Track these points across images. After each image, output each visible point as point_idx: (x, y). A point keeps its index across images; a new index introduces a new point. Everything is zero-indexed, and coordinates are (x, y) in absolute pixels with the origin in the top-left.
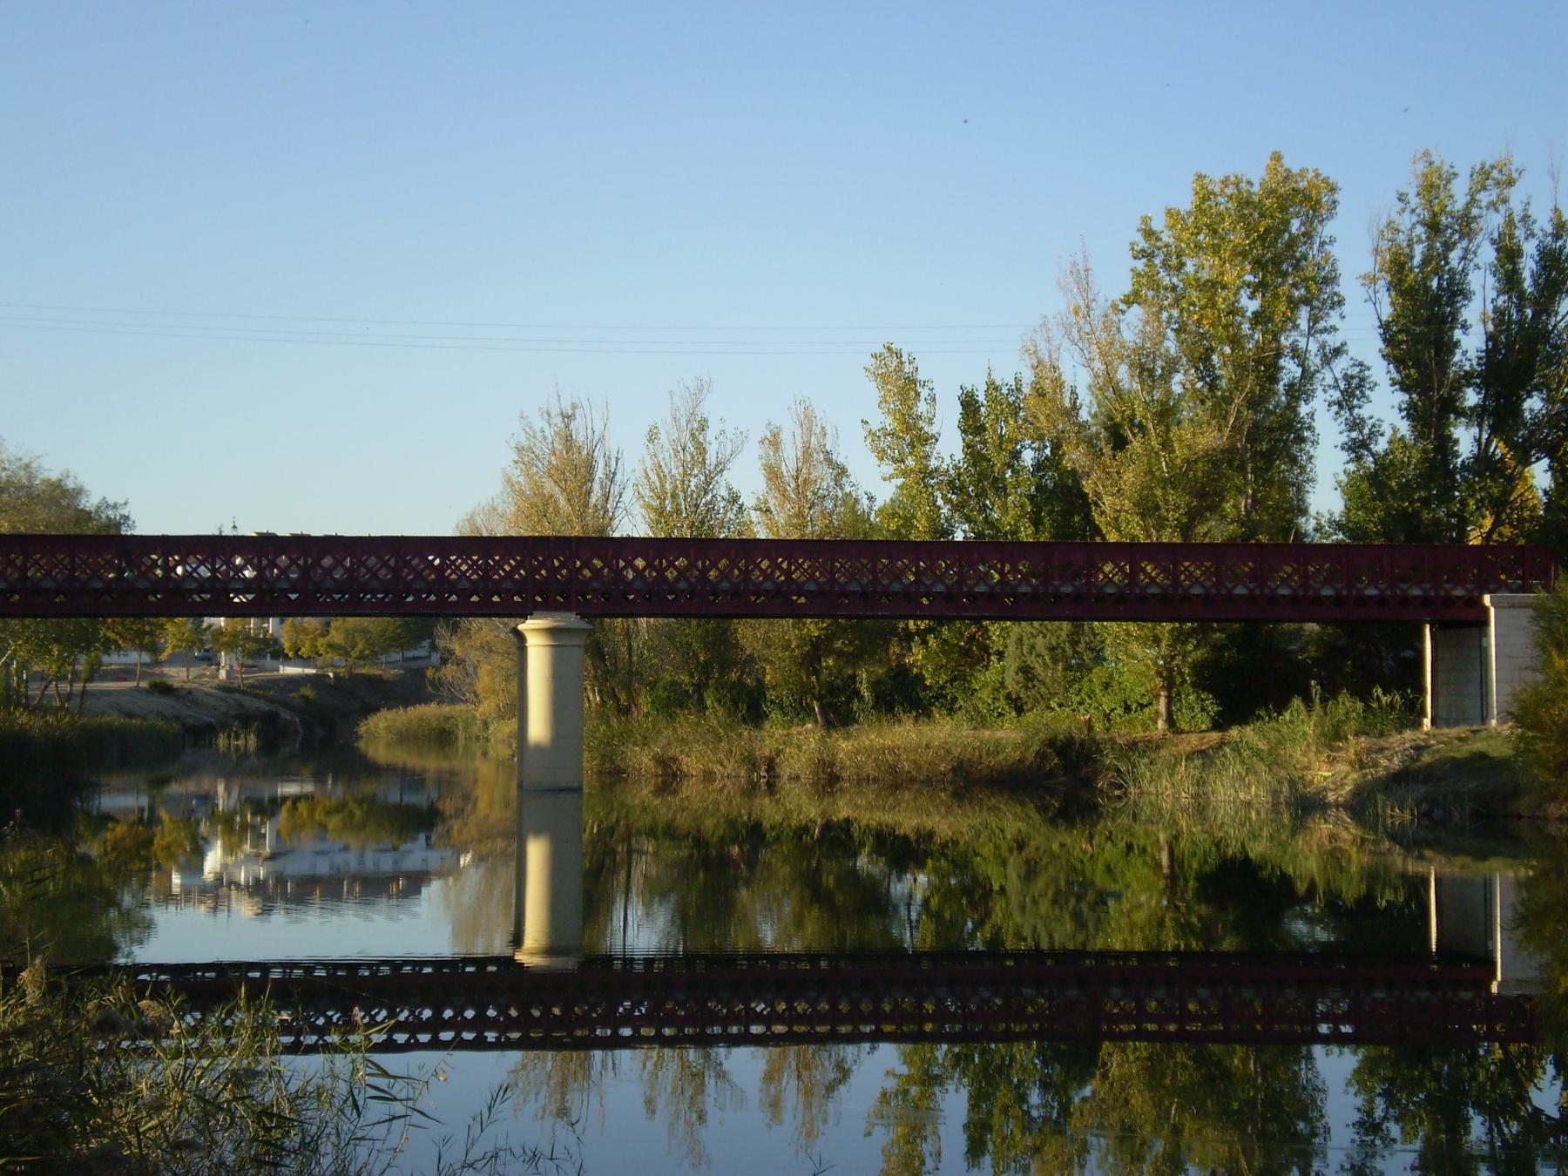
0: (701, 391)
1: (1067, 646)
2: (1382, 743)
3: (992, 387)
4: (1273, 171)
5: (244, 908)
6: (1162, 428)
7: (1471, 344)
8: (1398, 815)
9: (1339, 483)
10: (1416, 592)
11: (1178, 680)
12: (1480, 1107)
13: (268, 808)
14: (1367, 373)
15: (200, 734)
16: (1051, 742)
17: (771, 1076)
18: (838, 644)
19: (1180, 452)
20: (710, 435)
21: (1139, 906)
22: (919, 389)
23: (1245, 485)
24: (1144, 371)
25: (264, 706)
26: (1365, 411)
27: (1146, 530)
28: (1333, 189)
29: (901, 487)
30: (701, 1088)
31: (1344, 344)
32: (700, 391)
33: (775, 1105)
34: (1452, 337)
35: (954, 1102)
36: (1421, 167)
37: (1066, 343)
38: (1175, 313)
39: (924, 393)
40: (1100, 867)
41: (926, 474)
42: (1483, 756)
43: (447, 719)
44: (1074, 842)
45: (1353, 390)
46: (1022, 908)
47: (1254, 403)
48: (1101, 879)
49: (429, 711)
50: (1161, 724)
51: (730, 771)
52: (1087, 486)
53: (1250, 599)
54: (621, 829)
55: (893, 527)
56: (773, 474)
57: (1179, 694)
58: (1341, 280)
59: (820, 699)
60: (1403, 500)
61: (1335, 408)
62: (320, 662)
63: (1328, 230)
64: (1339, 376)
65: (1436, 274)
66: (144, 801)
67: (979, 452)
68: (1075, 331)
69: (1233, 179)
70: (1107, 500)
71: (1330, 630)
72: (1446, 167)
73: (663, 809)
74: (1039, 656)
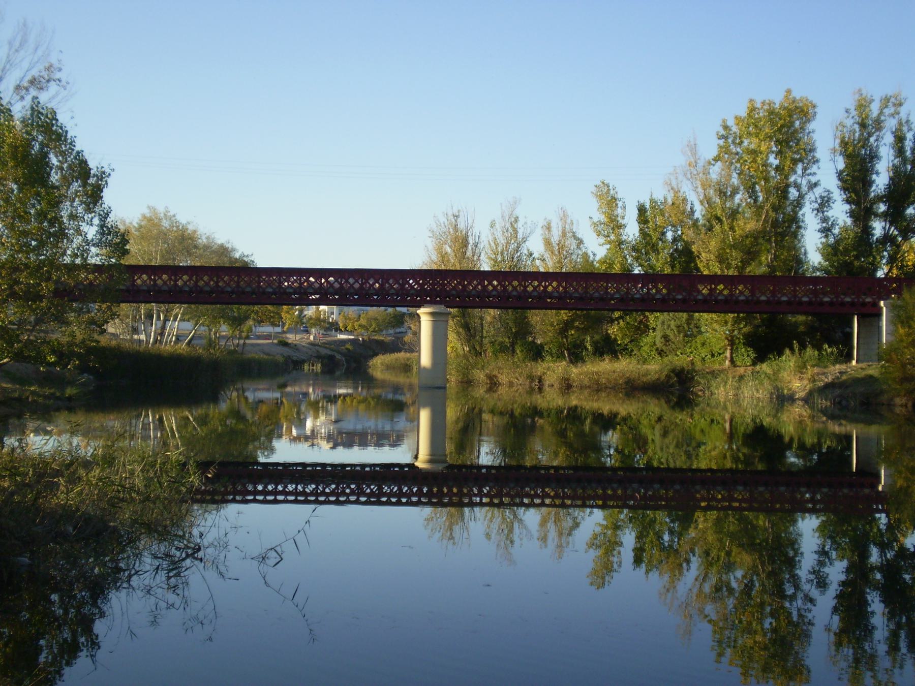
0: (515, 203)
1: (685, 326)
2: (826, 371)
3: (652, 201)
4: (787, 97)
5: (325, 445)
6: (730, 220)
7: (881, 181)
8: (824, 403)
9: (818, 248)
10: (848, 299)
11: (737, 341)
12: (875, 544)
13: (333, 399)
14: (831, 195)
15: (297, 364)
16: (673, 371)
17: (543, 523)
18: (577, 324)
19: (738, 232)
20: (520, 224)
21: (714, 448)
22: (618, 202)
23: (771, 248)
24: (722, 193)
25: (329, 352)
26: (829, 214)
27: (721, 269)
28: (814, 107)
29: (610, 249)
30: (511, 530)
31: (819, 181)
32: (515, 203)
33: (544, 539)
34: (871, 178)
35: (629, 538)
36: (857, 97)
37: (685, 179)
38: (738, 165)
39: (620, 204)
40: (698, 429)
41: (620, 243)
42: (871, 377)
43: (408, 359)
44: (680, 417)
45: (824, 203)
46: (662, 449)
47: (775, 209)
48: (698, 435)
49: (401, 355)
50: (727, 362)
51: (521, 382)
52: (694, 248)
53: (768, 302)
54: (477, 410)
55: (604, 268)
56: (548, 243)
57: (737, 348)
58: (818, 150)
59: (568, 349)
60: (846, 256)
61: (816, 212)
62: (355, 333)
63: (811, 126)
64: (818, 196)
65: (864, 148)
66: (277, 395)
67: (646, 233)
68: (689, 173)
69: (767, 101)
70: (703, 254)
71: (810, 318)
72: (869, 96)
73: (491, 400)
74: (672, 330)
